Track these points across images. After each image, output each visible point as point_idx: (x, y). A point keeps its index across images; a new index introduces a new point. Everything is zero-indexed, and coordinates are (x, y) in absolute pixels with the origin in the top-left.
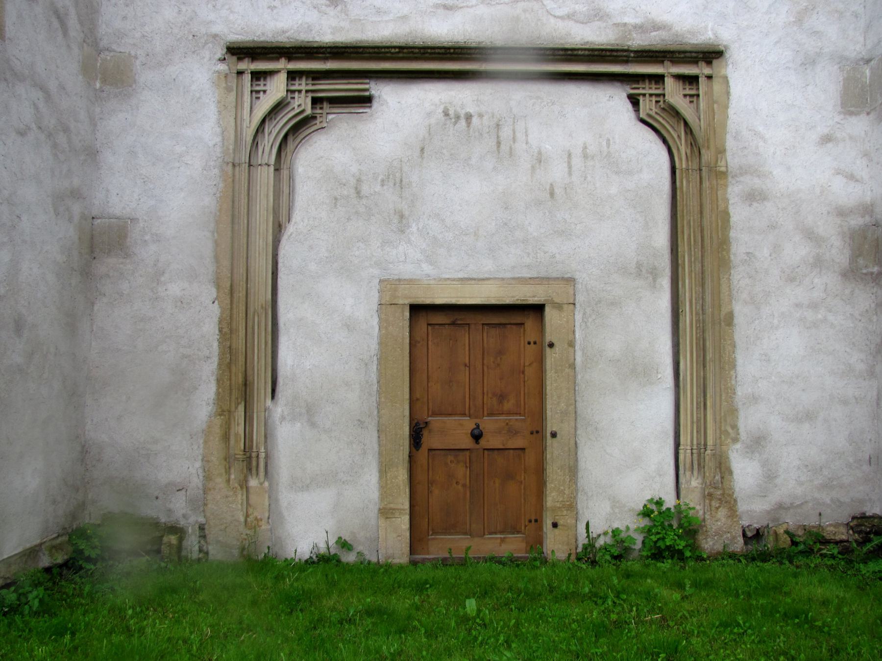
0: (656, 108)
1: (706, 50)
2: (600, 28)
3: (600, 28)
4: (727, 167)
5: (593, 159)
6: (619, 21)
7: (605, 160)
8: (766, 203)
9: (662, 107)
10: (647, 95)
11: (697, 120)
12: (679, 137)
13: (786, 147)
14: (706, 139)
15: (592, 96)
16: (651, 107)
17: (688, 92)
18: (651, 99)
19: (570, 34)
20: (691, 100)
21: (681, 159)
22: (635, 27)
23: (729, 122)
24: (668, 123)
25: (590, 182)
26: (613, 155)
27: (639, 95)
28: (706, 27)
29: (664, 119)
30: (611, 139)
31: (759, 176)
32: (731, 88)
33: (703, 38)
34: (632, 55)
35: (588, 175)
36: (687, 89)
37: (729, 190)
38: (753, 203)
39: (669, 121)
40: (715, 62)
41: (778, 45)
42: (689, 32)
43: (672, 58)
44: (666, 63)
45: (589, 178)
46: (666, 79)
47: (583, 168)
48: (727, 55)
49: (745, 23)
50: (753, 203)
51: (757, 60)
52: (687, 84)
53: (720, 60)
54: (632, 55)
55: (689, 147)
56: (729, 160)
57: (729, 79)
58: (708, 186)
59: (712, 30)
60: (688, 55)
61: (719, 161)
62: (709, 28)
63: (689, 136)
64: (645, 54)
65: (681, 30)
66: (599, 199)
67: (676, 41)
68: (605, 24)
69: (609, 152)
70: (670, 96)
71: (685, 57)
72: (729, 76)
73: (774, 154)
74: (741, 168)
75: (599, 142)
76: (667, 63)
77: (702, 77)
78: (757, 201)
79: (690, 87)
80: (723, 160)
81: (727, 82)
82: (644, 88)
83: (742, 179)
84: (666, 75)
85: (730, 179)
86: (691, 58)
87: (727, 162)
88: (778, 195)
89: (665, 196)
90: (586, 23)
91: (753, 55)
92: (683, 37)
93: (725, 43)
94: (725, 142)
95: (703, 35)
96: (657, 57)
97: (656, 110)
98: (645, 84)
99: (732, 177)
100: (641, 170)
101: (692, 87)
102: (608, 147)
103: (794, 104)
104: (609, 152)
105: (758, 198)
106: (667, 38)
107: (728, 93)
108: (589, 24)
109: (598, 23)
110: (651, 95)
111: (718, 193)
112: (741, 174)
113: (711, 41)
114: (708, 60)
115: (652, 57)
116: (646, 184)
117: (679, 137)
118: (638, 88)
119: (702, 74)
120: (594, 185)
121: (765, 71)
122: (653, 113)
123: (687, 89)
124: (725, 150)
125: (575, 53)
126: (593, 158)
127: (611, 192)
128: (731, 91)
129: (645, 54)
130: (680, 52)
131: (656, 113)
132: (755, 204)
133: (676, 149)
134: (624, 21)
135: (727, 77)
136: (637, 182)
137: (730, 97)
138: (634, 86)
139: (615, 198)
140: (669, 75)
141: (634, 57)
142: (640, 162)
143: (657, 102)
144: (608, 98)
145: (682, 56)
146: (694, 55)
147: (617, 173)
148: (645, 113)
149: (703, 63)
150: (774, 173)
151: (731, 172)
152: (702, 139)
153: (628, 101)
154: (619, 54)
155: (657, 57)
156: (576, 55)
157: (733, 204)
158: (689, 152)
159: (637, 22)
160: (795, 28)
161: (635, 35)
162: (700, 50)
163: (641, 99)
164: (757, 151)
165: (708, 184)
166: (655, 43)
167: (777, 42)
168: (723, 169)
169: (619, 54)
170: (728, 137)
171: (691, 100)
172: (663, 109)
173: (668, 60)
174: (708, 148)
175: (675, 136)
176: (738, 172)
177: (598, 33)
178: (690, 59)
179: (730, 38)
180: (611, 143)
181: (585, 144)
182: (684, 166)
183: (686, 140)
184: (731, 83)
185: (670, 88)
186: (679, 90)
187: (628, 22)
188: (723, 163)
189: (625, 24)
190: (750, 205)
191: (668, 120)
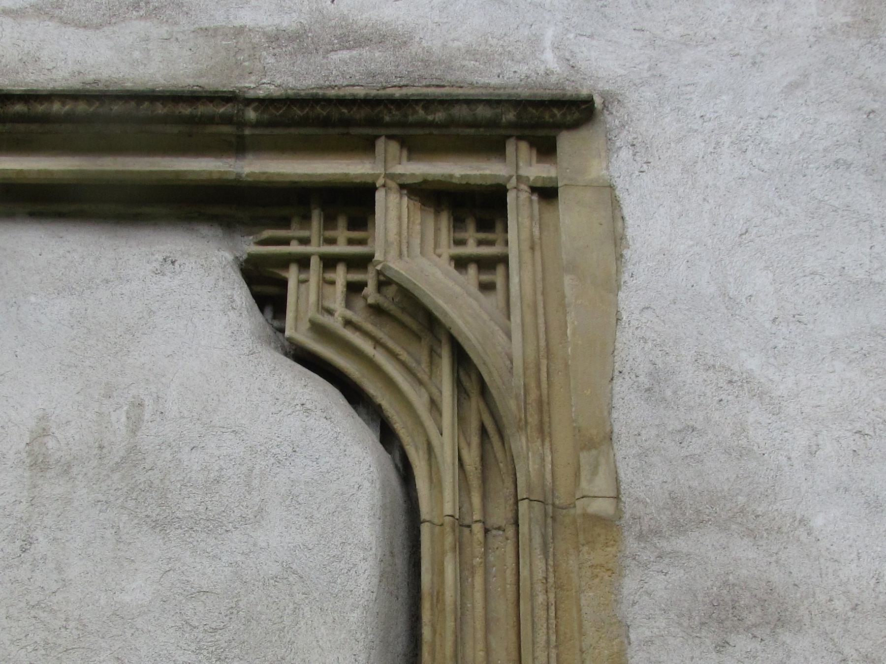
0: (348, 305)
1: (524, 93)
2: (147, 39)
3: (147, 39)
4: (617, 498)
5: (66, 472)
6: (219, 18)
7: (116, 476)
8: (786, 637)
9: (371, 300)
10: (315, 262)
11: (501, 337)
12: (434, 405)
13: (858, 426)
14: (533, 395)
15: (97, 260)
16: (328, 304)
17: (471, 249)
18: (329, 276)
19: (37, 60)
20: (486, 278)
21: (435, 482)
22: (275, 38)
23: (625, 337)
24: (394, 355)
25: (44, 558)
26: (150, 460)
27: (285, 262)
28: (535, 42)
29: (377, 343)
30: (148, 402)
31: (751, 534)
32: (629, 221)
33: (523, 69)
34: (251, 114)
35: (38, 534)
36: (471, 242)
37: (630, 584)
38: (733, 638)
39: (398, 349)
40: (566, 142)
41: (799, 93)
42: (471, 52)
43: (404, 125)
44: (380, 144)
45: (42, 546)
46: (379, 195)
47: (24, 505)
48: (612, 120)
49: (678, 30)
50: (733, 638)
51: (726, 139)
52: (471, 227)
53: (583, 133)
54: (251, 114)
55: (475, 440)
56: (625, 474)
57: (620, 194)
58: (539, 575)
59: (556, 48)
60: (461, 112)
61: (585, 474)
62: (547, 44)
63: (475, 403)
64: (298, 112)
65: (444, 46)
66: (72, 624)
67: (421, 77)
68: (165, 28)
69: (133, 449)
70: (393, 252)
71: (451, 123)
72: (620, 184)
73: (812, 454)
74: (675, 501)
75: (100, 414)
76: (386, 148)
77: (633, 326)
78: (747, 629)
79: (482, 236)
80: (602, 469)
81: (615, 204)
82: (305, 241)
83: (681, 544)
84: (380, 182)
85: (631, 545)
86: (475, 124)
87: (617, 480)
88: (839, 605)
89: (355, 616)
90: (98, 27)
91: (709, 126)
92: (450, 68)
93: (601, 86)
94: (611, 408)
95: (524, 60)
96: (347, 123)
97: (349, 314)
98: (309, 228)
99: (641, 537)
100: (260, 512)
101: (490, 236)
102: (134, 432)
103: (876, 278)
104: (133, 449)
105: (751, 619)
106: (390, 68)
107: (618, 240)
108: (108, 30)
109: (140, 26)
110: (329, 262)
111: (583, 602)
112: (679, 528)
113: (553, 79)
114: (541, 133)
115: (325, 123)
116: (275, 569)
117: (434, 405)
118: (286, 242)
119: (519, 178)
120: (59, 569)
121: (755, 172)
122: (335, 323)
123: (471, 242)
124: (609, 437)
125: (40, 108)
126: (66, 470)
127: (127, 598)
128: (630, 233)
129: (298, 112)
130: (428, 103)
131: (348, 323)
132: (742, 643)
133: (423, 447)
134: (238, 23)
135: (612, 187)
136: (239, 558)
137: (627, 253)
138: (267, 234)
139: (139, 622)
140: (392, 184)
141: (258, 124)
142: (256, 483)
143: (354, 288)
144: (156, 265)
145: (440, 116)
146: (483, 112)
147: (159, 526)
148: (305, 326)
149: (524, 146)
150: (818, 522)
151: (636, 519)
152: (517, 397)
153: (237, 278)
154: (202, 109)
155: (347, 123)
156: (45, 119)
157: (650, 642)
158: (472, 458)
159: (285, 24)
160: (854, 44)
161: (271, 60)
162: (503, 93)
163: (292, 275)
164: (744, 442)
165: (539, 564)
166: (340, 81)
167: (793, 86)
168: (603, 507)
169: (202, 109)
170: (621, 387)
171: (486, 278)
172: (377, 310)
173: (389, 137)
174: (543, 431)
175: (419, 401)
176: (665, 517)
177: (137, 54)
178: (471, 131)
179: (623, 72)
180: (147, 416)
181: (44, 418)
182: (448, 509)
183: (461, 419)
184: (630, 206)
185: (393, 226)
186: (436, 245)
187: (250, 24)
188: (601, 484)
189: (240, 31)
190: (722, 646)
191: (391, 344)
